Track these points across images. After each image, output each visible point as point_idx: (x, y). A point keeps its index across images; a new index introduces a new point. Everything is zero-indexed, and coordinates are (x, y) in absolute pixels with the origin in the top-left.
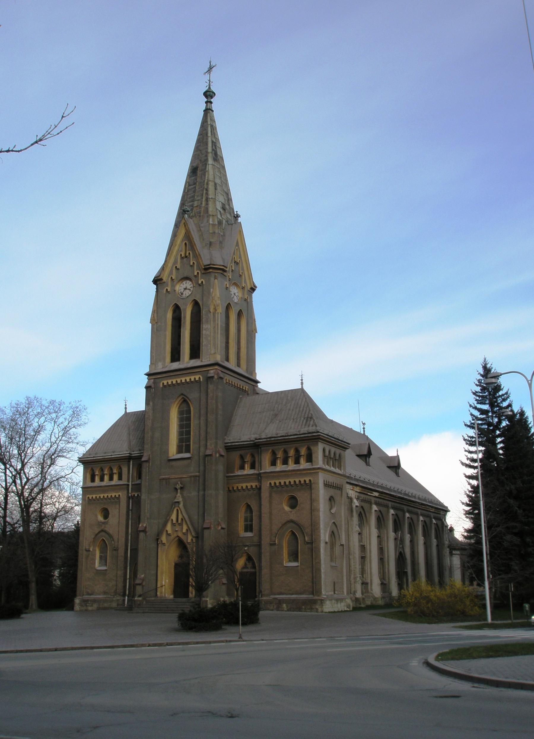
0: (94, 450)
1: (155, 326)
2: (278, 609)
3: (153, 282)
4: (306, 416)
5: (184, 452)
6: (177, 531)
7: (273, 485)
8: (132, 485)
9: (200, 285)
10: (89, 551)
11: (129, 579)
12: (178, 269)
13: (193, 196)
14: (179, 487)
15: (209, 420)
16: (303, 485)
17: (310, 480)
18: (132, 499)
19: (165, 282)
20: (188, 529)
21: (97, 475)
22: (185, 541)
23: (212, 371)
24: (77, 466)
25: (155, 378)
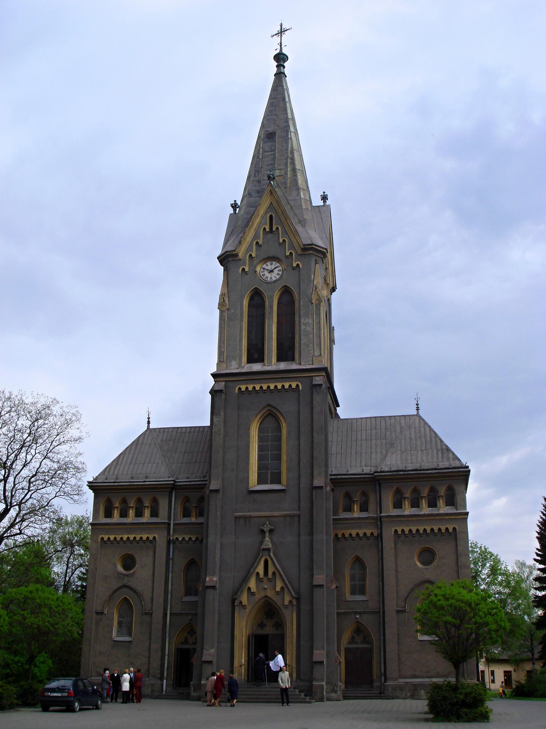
0: (111, 473)
1: (226, 314)
2: (412, 697)
3: (218, 258)
4: (439, 447)
5: (269, 483)
6: (265, 589)
7: (400, 532)
8: (174, 525)
9: (294, 269)
10: (102, 613)
11: (168, 655)
12: (260, 246)
13: (273, 164)
14: (268, 529)
15: (315, 440)
16: (451, 534)
17: (454, 529)
18: (174, 544)
19: (241, 260)
20: (284, 586)
21: (117, 508)
22: (279, 604)
23: (318, 378)
24: (55, 497)
25: (226, 381)
